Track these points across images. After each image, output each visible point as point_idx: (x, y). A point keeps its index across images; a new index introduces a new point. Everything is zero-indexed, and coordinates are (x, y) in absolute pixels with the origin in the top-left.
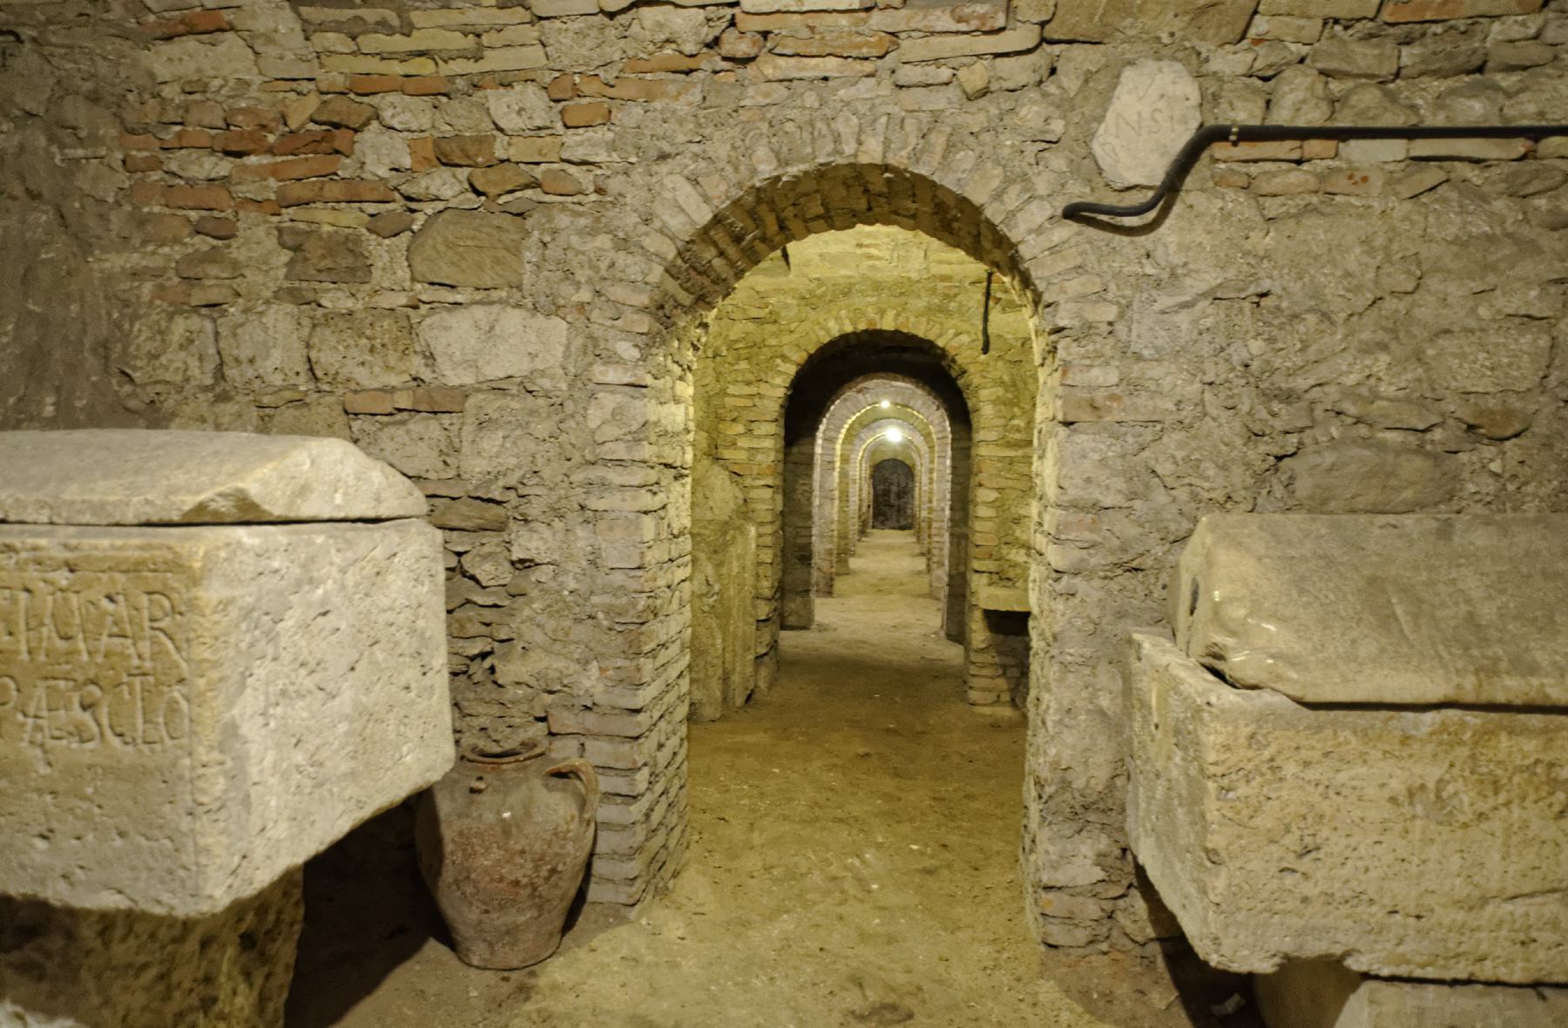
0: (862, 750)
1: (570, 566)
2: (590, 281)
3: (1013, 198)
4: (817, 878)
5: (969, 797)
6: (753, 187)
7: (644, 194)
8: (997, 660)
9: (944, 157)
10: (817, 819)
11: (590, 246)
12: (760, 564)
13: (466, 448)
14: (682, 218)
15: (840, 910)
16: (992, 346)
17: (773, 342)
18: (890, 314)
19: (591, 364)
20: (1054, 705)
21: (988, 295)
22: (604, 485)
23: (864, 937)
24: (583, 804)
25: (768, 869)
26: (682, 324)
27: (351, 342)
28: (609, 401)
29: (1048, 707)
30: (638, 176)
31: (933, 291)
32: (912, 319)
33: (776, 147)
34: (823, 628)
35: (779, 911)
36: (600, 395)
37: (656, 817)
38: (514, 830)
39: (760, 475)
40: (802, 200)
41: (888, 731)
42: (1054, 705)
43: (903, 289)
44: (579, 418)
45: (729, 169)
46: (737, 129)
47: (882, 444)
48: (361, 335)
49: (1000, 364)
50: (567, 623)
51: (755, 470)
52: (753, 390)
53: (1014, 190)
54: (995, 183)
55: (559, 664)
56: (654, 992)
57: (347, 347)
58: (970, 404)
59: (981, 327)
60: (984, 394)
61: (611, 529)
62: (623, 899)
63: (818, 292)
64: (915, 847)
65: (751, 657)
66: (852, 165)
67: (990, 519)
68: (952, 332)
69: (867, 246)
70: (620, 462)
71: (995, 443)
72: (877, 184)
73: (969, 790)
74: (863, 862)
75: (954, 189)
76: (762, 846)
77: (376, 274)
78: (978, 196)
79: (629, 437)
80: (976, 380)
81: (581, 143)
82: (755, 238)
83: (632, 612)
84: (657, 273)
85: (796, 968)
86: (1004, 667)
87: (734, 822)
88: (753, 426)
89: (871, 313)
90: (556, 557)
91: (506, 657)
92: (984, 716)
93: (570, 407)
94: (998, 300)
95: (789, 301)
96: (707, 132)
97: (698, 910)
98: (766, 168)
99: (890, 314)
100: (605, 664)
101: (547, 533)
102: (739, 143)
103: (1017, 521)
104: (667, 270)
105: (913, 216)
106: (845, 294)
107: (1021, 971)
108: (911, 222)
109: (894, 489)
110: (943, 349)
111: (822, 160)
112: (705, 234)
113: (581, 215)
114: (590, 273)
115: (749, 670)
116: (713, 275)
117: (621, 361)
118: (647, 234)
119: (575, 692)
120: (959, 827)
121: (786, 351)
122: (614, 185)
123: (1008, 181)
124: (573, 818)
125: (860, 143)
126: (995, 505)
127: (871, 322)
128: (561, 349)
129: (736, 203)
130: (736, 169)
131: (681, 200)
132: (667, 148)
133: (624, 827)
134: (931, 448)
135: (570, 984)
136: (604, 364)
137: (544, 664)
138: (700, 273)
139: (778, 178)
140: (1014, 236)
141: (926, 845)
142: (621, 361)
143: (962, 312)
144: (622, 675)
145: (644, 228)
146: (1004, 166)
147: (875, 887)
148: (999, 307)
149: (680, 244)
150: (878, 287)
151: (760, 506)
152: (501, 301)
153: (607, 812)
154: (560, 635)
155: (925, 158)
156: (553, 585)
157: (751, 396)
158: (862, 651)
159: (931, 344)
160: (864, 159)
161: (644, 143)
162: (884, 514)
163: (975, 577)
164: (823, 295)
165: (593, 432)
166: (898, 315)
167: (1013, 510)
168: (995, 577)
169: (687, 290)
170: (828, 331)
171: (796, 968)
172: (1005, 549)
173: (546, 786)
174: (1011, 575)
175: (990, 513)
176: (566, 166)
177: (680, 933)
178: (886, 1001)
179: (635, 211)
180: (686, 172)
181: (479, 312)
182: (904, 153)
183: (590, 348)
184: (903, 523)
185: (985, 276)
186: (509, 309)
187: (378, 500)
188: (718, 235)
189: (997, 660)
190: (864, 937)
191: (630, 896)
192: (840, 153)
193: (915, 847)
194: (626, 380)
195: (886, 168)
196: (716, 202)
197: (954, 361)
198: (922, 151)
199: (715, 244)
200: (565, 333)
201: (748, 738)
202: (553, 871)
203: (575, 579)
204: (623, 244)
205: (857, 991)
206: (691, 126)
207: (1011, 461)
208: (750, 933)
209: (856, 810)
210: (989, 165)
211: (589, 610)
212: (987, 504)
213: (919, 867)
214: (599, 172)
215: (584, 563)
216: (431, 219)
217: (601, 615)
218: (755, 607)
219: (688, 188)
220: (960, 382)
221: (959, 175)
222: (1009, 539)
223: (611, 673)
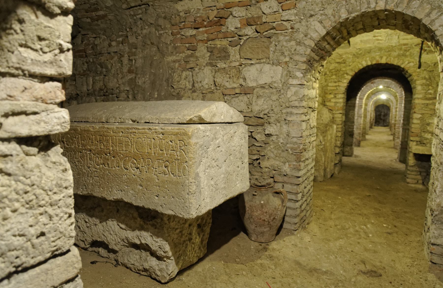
0: (368, 194)
1: (281, 136)
2: (289, 55)
3: (434, 15)
4: (351, 230)
5: (405, 212)
6: (340, 22)
7: (305, 28)
8: (418, 169)
9: (408, 4)
10: (352, 213)
11: (289, 45)
12: (337, 136)
13: (254, 103)
14: (317, 34)
15: (359, 241)
16: (422, 66)
17: (344, 69)
18: (384, 58)
19: (288, 79)
20: (439, 186)
21: (421, 49)
22: (291, 113)
23: (366, 250)
24: (283, 201)
25: (336, 226)
26: (315, 66)
27: (225, 76)
28: (293, 89)
29: (437, 186)
30: (303, 23)
31: (401, 49)
32: (392, 59)
33: (348, 9)
34: (356, 156)
35: (339, 238)
36: (291, 88)
37: (303, 207)
38: (264, 206)
39: (338, 110)
40: (356, 24)
41: (377, 189)
42: (439, 186)
43: (390, 49)
44: (285, 94)
45: (332, 17)
46: (335, 4)
47: (379, 99)
48: (227, 74)
49: (425, 72)
50: (280, 152)
51: (337, 108)
52: (337, 84)
53: (434, 12)
54: (427, 11)
55: (278, 163)
56: (301, 255)
57: (224, 77)
58: (412, 86)
59: (418, 60)
60: (418, 82)
61: (293, 126)
62: (293, 228)
63: (359, 53)
64: (385, 225)
65: (333, 164)
66: (373, 11)
67: (418, 124)
68: (407, 62)
69: (377, 36)
70: (296, 107)
71: (422, 99)
72: (382, 16)
73: (405, 210)
74: (367, 227)
75: (411, 14)
76: (334, 219)
77: (231, 57)
78: (419, 16)
79: (299, 100)
80: (415, 78)
81: (286, 15)
82: (339, 38)
83: (298, 149)
84: (309, 50)
85: (344, 255)
86: (421, 172)
87: (326, 211)
88: (336, 95)
89: (378, 58)
90: (277, 133)
91: (263, 160)
92: (412, 187)
93: (282, 91)
94: (425, 50)
95: (350, 56)
96: (325, 7)
97: (314, 234)
98: (344, 15)
99: (384, 58)
100: (290, 163)
101: (275, 127)
102: (336, 9)
103: (428, 124)
104: (312, 50)
105: (395, 25)
106: (369, 53)
107: (421, 269)
108: (394, 27)
109: (383, 114)
110: (403, 68)
111: (363, 11)
112: (323, 38)
113: (286, 36)
114: (289, 53)
115: (332, 168)
116: (326, 50)
117: (297, 78)
118: (306, 40)
119: (282, 171)
120: (401, 221)
121: (348, 72)
122: (296, 26)
123: (432, 9)
124: (280, 205)
125: (377, 3)
126: (421, 119)
127: (377, 61)
128: (280, 75)
129: (334, 28)
130: (334, 17)
131: (317, 28)
132: (312, 13)
133: (294, 209)
134: (397, 101)
135: (277, 249)
136: (293, 79)
137: (273, 163)
138: (322, 50)
139: (348, 18)
140: (433, 28)
141: (389, 225)
142: (297, 78)
143: (411, 55)
144: (295, 167)
145: (305, 38)
146: (431, 4)
147: (370, 235)
148: (426, 53)
149: (316, 42)
150: (380, 49)
151: (338, 119)
152: (264, 63)
153: (289, 204)
154: (278, 155)
155: (400, 5)
156: (276, 141)
157: (336, 86)
158: (370, 164)
159: (399, 67)
160: (378, 9)
161: (306, 12)
162: (379, 122)
163: (411, 143)
164: (361, 54)
165: (289, 98)
166: (387, 58)
167: (427, 121)
168: (419, 143)
169: (318, 56)
170: (362, 65)
171: (344, 255)
172: (423, 134)
173: (273, 196)
174: (425, 142)
175: (419, 122)
176: (282, 22)
177: (309, 240)
178: (373, 269)
179: (303, 33)
180: (318, 20)
181: (258, 66)
182: (393, 5)
183: (288, 74)
184: (385, 124)
185: (421, 42)
186: (266, 64)
187: (232, 118)
188: (328, 38)
189: (418, 169)
190: (366, 250)
191: (295, 228)
192: (369, 8)
193: (385, 225)
194: (299, 83)
195: (386, 10)
196: (328, 28)
197: (407, 72)
198: (399, 4)
199: (327, 41)
200: (281, 70)
201: (331, 187)
202: (274, 218)
203: (283, 140)
204: (299, 43)
205: (363, 265)
206: (320, 5)
207: (427, 105)
208: (330, 243)
209: (365, 212)
210: (425, 4)
211: (286, 148)
212: (416, 119)
213: (385, 231)
214: (292, 23)
215: (285, 135)
216: (245, 41)
217: (289, 150)
218: (335, 149)
219: (319, 24)
220: (409, 79)
221: (413, 10)
222: (425, 130)
223: (292, 166)
